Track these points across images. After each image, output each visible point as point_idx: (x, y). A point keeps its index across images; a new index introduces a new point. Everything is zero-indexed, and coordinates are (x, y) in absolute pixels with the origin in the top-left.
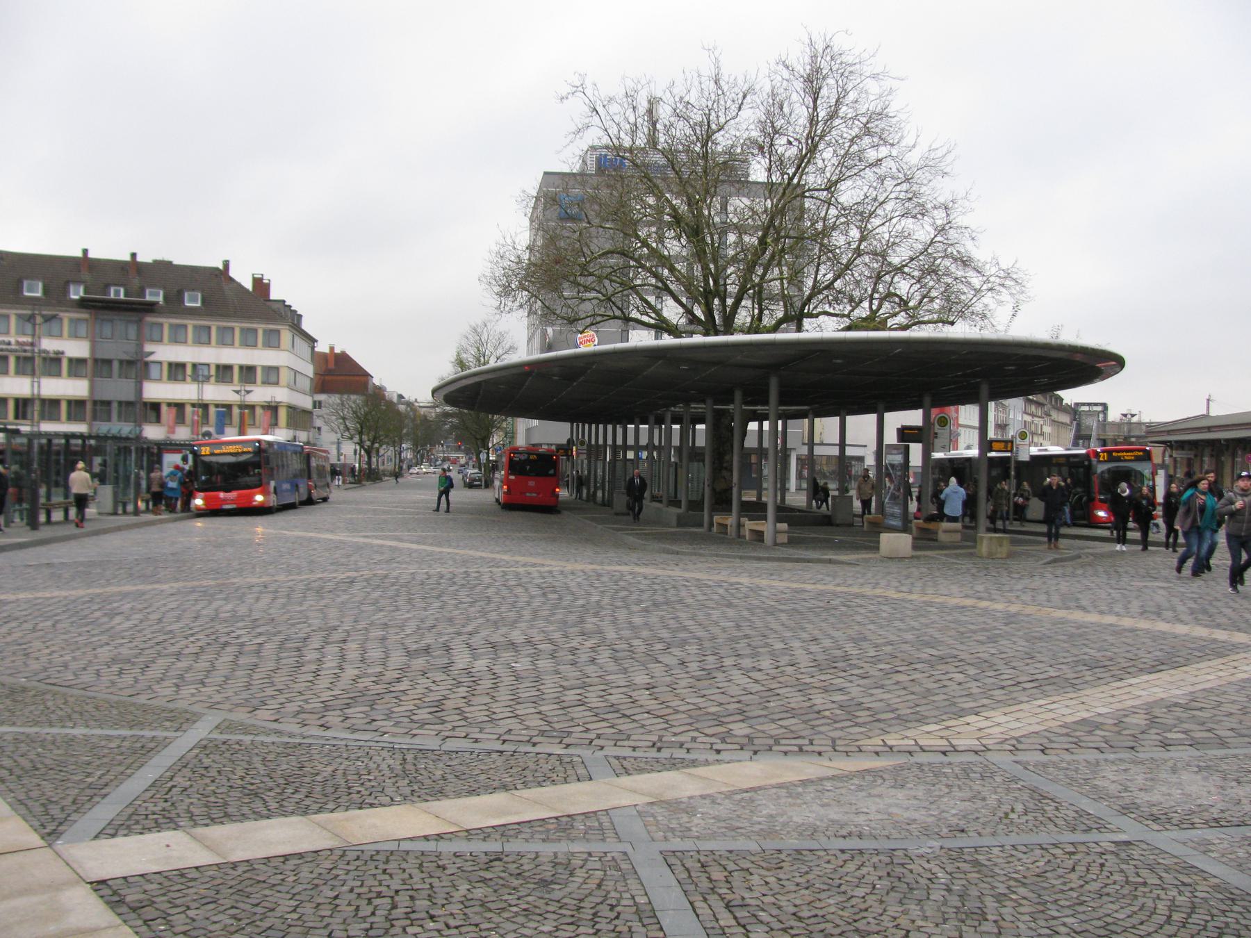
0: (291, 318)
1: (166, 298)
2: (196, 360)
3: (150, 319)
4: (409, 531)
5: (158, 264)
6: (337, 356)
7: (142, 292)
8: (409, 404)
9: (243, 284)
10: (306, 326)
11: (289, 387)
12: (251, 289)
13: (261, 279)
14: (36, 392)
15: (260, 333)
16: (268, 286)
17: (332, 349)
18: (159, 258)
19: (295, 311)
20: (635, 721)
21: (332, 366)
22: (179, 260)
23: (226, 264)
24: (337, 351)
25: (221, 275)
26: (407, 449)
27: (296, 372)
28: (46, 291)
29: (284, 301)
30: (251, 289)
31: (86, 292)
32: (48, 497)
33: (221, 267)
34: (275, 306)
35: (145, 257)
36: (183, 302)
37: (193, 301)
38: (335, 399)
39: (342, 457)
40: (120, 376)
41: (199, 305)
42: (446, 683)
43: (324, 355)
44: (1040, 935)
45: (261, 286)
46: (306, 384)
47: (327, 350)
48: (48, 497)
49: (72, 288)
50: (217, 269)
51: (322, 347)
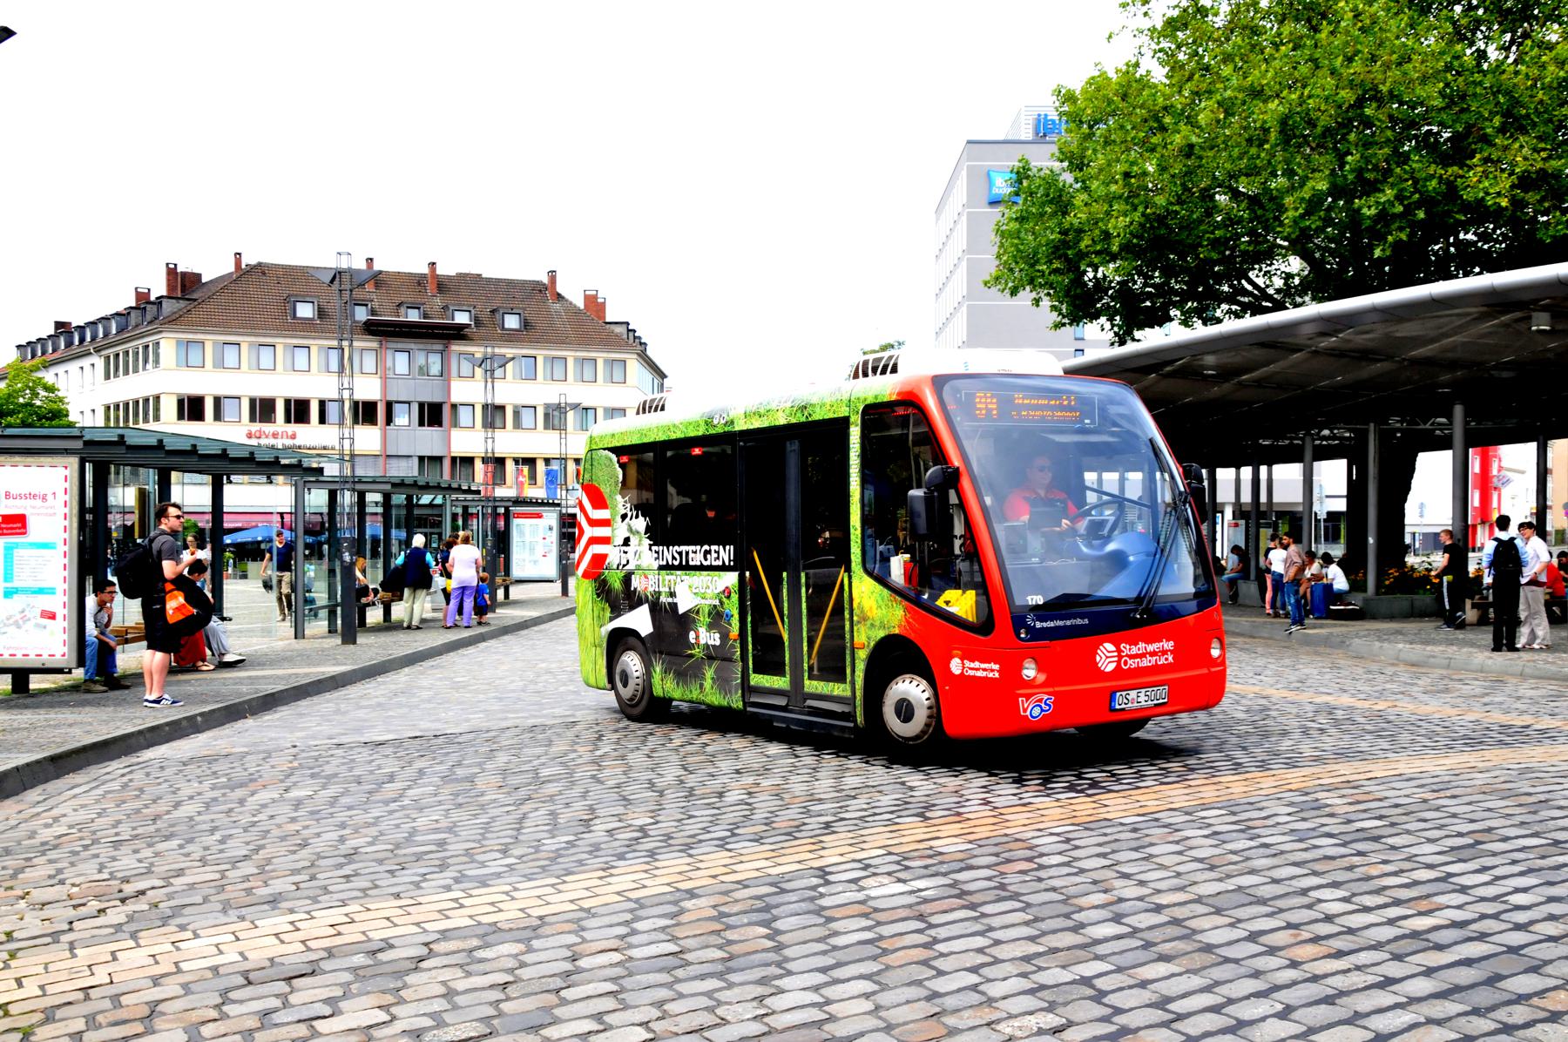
0: (629, 340)
2: (220, 392)
3: (457, 347)
5: (462, 278)
12: (582, 307)
13: (595, 297)
14: (563, 452)
15: (600, 363)
22: (489, 272)
23: (552, 275)
25: (544, 291)
29: (628, 324)
30: (582, 307)
33: (545, 280)
35: (446, 269)
40: (546, 427)
42: (769, 804)
44: (1507, 1029)
45: (594, 304)
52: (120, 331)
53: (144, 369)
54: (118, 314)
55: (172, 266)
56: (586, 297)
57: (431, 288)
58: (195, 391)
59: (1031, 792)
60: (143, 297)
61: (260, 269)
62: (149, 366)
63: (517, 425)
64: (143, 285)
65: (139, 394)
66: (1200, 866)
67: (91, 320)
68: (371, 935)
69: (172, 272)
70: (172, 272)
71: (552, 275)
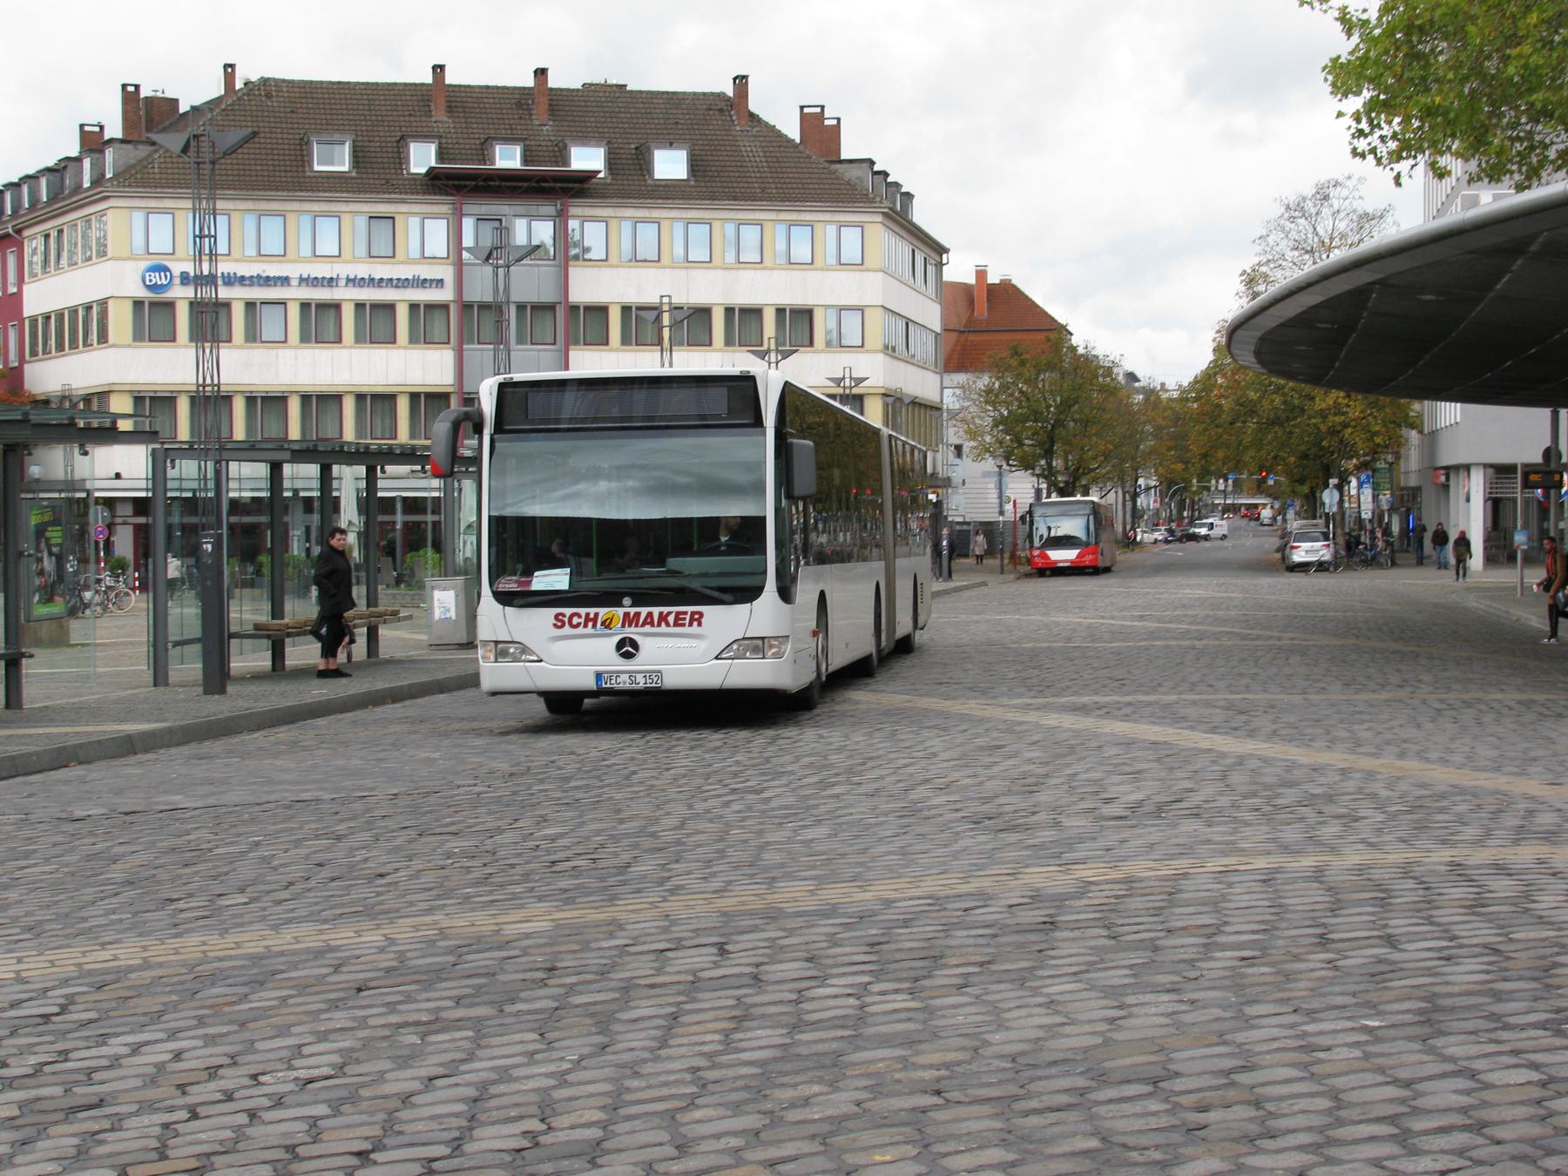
1: (611, 163)
2: (634, 297)
4: (1193, 687)
6: (992, 289)
7: (484, 154)
8: (1149, 393)
9: (784, 131)
10: (921, 216)
11: (889, 350)
12: (798, 141)
16: (836, 129)
17: (981, 274)
18: (598, 79)
19: (897, 185)
20: (1381, 1070)
21: (982, 311)
23: (741, 82)
24: (993, 278)
26: (1148, 489)
27: (908, 322)
28: (358, 158)
31: (441, 156)
32: (372, 600)
34: (852, 173)
36: (311, 165)
37: (670, 164)
38: (961, 378)
39: (1009, 507)
41: (345, 168)
43: (965, 288)
46: (924, 346)
47: (971, 279)
48: (372, 600)
49: (499, 149)
50: (720, 96)
51: (959, 270)
52: (53, 199)
53: (57, 267)
54: (49, 170)
55: (131, 89)
56: (804, 118)
57: (540, 113)
58: (698, 298)
59: (790, 732)
60: (93, 141)
61: (266, 88)
62: (64, 261)
63: (253, 336)
64: (91, 118)
65: (77, 298)
66: (1512, 1020)
67: (31, 171)
68: (209, 954)
69: (130, 96)
70: (130, 96)
71: (741, 82)
